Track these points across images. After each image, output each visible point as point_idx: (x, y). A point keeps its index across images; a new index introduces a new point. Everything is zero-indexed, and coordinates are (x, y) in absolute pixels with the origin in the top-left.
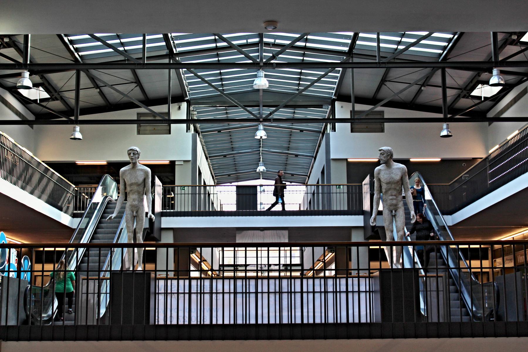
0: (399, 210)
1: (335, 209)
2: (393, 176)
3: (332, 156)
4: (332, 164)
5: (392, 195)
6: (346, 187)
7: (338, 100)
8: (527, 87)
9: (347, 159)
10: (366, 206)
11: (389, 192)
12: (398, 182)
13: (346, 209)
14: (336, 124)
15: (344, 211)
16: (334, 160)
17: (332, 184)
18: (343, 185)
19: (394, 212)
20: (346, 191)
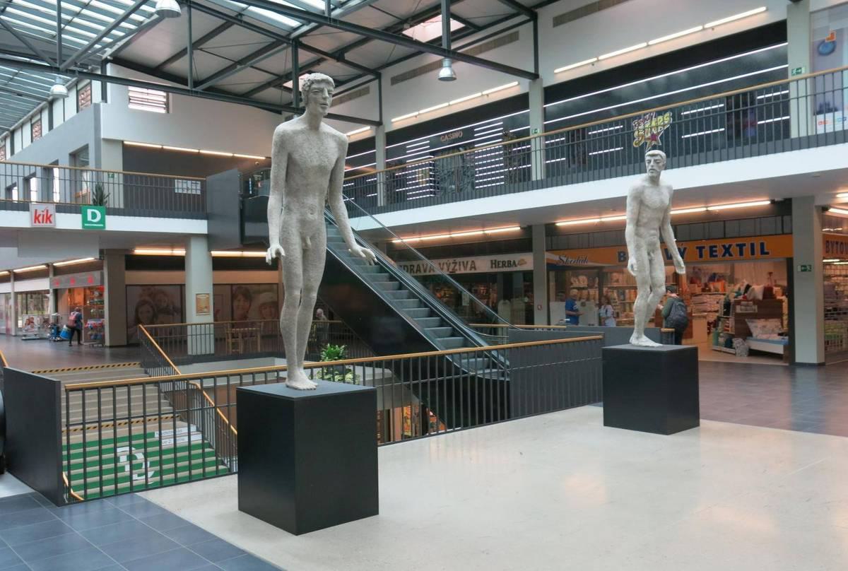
3: (103, 135)
6: (121, 175)
9: (123, 142)
13: (122, 206)
15: (119, 209)
16: (107, 141)
17: (103, 169)
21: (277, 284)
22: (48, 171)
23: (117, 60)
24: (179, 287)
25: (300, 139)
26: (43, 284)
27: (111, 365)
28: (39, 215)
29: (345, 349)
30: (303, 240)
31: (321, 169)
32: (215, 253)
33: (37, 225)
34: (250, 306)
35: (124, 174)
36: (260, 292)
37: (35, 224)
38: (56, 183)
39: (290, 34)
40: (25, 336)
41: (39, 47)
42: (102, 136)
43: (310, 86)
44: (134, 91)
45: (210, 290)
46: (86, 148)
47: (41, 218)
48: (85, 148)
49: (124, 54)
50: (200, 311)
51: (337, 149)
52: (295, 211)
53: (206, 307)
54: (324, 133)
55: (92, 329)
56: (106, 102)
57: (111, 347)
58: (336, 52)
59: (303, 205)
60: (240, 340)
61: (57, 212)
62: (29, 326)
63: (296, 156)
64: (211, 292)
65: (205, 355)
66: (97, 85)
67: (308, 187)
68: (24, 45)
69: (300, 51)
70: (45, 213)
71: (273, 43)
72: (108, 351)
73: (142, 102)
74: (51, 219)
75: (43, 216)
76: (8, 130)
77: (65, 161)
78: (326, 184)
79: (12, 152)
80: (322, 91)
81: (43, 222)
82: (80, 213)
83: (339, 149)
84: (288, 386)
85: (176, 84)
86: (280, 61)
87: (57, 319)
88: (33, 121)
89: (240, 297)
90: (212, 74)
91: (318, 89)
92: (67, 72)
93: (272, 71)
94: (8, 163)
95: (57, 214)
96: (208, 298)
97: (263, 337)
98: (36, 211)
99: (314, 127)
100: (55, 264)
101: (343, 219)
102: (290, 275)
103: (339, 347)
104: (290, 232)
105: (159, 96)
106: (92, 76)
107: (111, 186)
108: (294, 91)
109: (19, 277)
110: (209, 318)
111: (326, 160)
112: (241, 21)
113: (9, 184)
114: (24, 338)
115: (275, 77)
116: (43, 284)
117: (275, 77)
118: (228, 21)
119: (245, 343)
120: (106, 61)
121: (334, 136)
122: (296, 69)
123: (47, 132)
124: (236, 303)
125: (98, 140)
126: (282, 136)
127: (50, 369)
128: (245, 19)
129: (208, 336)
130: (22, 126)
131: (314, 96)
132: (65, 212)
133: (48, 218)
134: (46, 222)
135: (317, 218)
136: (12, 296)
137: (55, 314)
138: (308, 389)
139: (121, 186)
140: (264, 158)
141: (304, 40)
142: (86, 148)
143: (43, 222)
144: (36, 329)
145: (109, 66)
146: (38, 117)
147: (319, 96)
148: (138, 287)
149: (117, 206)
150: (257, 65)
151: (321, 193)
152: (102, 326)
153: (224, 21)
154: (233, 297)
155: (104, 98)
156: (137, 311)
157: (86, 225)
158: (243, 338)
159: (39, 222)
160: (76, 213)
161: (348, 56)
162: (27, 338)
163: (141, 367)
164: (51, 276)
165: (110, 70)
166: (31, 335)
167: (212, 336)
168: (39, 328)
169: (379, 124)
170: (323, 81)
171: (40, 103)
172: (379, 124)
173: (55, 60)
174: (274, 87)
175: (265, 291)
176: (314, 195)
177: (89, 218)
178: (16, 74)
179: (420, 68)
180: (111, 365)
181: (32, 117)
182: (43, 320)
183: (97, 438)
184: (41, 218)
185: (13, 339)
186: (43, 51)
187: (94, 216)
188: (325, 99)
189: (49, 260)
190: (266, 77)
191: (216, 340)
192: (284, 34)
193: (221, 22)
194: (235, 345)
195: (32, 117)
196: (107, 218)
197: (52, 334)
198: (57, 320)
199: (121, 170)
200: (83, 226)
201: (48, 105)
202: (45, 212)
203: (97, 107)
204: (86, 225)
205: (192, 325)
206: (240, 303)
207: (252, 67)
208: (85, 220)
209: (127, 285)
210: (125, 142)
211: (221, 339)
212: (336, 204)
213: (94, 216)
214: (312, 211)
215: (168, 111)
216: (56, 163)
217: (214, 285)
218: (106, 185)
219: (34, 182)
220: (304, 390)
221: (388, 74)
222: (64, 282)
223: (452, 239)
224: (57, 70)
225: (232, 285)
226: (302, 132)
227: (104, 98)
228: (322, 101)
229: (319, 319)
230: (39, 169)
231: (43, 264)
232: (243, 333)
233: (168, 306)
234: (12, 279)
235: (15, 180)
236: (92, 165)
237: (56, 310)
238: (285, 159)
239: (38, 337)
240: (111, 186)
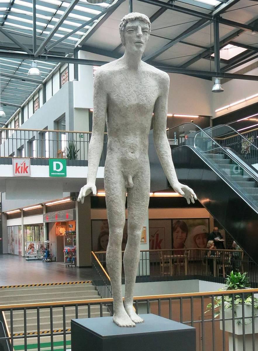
3: (75, 106)
9: (89, 109)
16: (77, 109)
17: (75, 131)
21: (209, 219)
22: (42, 134)
23: (85, 47)
25: (117, 79)
26: (39, 219)
27: (83, 281)
28: (19, 167)
29: (246, 275)
30: (126, 178)
31: (140, 109)
33: (18, 175)
34: (187, 236)
36: (195, 225)
37: (16, 174)
38: (47, 142)
39: (213, 11)
40: (28, 257)
41: (21, 41)
42: (74, 106)
43: (125, 26)
46: (64, 116)
47: (20, 170)
48: (63, 117)
49: (90, 41)
51: (157, 88)
52: (116, 150)
54: (144, 72)
55: (68, 253)
56: (77, 80)
57: (80, 267)
58: (252, 23)
59: (123, 144)
60: (170, 264)
61: (31, 165)
62: (31, 250)
63: (114, 97)
65: (141, 277)
66: (72, 66)
67: (128, 127)
68: (13, 42)
69: (221, 25)
70: (23, 166)
71: (200, 20)
72: (78, 270)
74: (28, 170)
75: (22, 167)
76: (20, 107)
77: (51, 127)
78: (148, 124)
79: (23, 122)
80: (136, 29)
81: (22, 173)
82: (48, 165)
83: (160, 88)
84: (114, 322)
86: (204, 36)
87: (48, 245)
88: (34, 100)
89: (179, 229)
91: (132, 27)
92: (40, 57)
94: (35, 131)
95: (32, 166)
96: (145, 230)
97: (190, 262)
98: (17, 164)
99: (133, 67)
100: (46, 204)
101: (166, 158)
102: (112, 213)
103: (242, 274)
104: (111, 171)
106: (69, 60)
108: (216, 59)
109: (26, 214)
111: (144, 98)
112: (172, 5)
113: (19, 146)
114: (27, 259)
115: (204, 50)
116: (39, 219)
117: (204, 50)
118: (163, 7)
119: (175, 268)
120: (77, 49)
121: (154, 75)
122: (217, 43)
123: (42, 105)
124: (175, 234)
125: (71, 109)
126: (99, 77)
127: (63, 282)
129: (144, 261)
130: (28, 104)
131: (129, 35)
132: (80, 166)
133: (25, 170)
134: (24, 173)
135: (140, 157)
136: (22, 227)
137: (46, 242)
138: (127, 327)
140: (197, 117)
141: (224, 16)
142: (64, 116)
143: (22, 173)
144: (36, 253)
146: (37, 96)
147: (134, 34)
148: (100, 222)
150: (185, 40)
151: (143, 132)
152: (75, 251)
153: (160, 7)
154: (173, 229)
155: (76, 77)
156: (99, 239)
157: (52, 174)
158: (173, 263)
159: (19, 173)
160: (45, 165)
162: (30, 259)
163: (93, 285)
164: (44, 213)
165: (81, 55)
166: (32, 256)
167: (148, 261)
168: (38, 251)
170: (136, 19)
171: (38, 85)
173: (31, 50)
174: (204, 58)
175: (199, 224)
176: (135, 134)
177: (55, 169)
178: (20, 65)
180: (83, 281)
181: (34, 95)
182: (40, 246)
183: (36, 342)
184: (20, 170)
185: (23, 259)
186: (23, 44)
187: (58, 166)
188: (139, 37)
189: (43, 201)
190: (196, 51)
191: (151, 264)
192: (207, 12)
194: (167, 269)
195: (34, 95)
196: (68, 168)
197: (45, 256)
198: (48, 246)
200: (50, 175)
201: (42, 86)
202: (23, 164)
203: (71, 84)
204: (52, 174)
206: (179, 234)
207: (180, 42)
208: (51, 170)
209: (92, 220)
211: (155, 263)
212: (160, 142)
213: (58, 166)
214: (133, 149)
216: (46, 128)
217: (149, 219)
219: (35, 143)
220: (124, 326)
222: (52, 217)
223: (168, 165)
224: (32, 57)
225: (172, 220)
226: (120, 72)
227: (76, 77)
228: (136, 39)
229: (235, 249)
230: (35, 134)
231: (39, 205)
232: (173, 260)
234: (22, 216)
235: (23, 143)
236: (67, 129)
237: (48, 239)
238: (104, 99)
239: (36, 258)
240: (82, 143)
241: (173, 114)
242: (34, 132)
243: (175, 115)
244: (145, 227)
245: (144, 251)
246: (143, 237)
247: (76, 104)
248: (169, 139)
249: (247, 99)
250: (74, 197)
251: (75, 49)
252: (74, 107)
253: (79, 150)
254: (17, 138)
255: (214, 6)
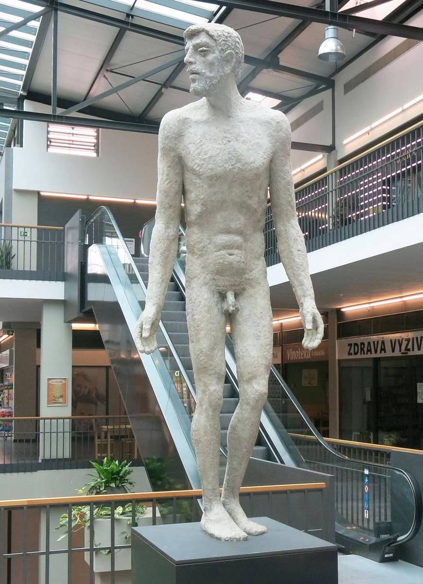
0: (250, 291)
1: (21, 268)
2: (241, 148)
3: (15, 186)
4: (15, 198)
5: (228, 232)
6: (35, 231)
7: (27, 97)
8: (272, 108)
9: (39, 193)
10: (71, 264)
11: (219, 217)
12: (257, 176)
13: (34, 268)
14: (25, 121)
15: (31, 272)
16: (18, 191)
17: (13, 224)
18: (48, 132)
19: (230, 297)
20: (35, 238)
23: (33, 95)
24: (105, 369)
32: (76, 326)
35: (38, 229)
42: (14, 187)
44: (58, 131)
45: (68, 375)
50: (52, 401)
53: (61, 396)
64: (69, 377)
65: (60, 460)
73: (71, 144)
85: (94, 117)
90: (153, 97)
93: (275, 91)
94: (14, 226)
105: (92, 132)
107: (21, 243)
110: (66, 411)
118: (121, 28)
120: (21, 99)
128: (136, 21)
129: (60, 435)
139: (34, 245)
145: (26, 102)
149: (27, 269)
161: (285, 58)
169: (330, 149)
172: (330, 149)
179: (378, 62)
193: (372, 39)
199: (35, 224)
205: (44, 419)
210: (42, 193)
215: (97, 152)
218: (14, 243)
221: (341, 79)
233: (89, 392)
241: (135, 200)
242: (32, 229)
243: (138, 201)
244: (66, 379)
245: (66, 419)
246: (61, 394)
247: (18, 183)
248: (126, 239)
249: (303, 167)
250: (10, 330)
251: (18, 99)
252: (13, 188)
253: (15, 255)
254: (32, 240)
255: (213, 12)
